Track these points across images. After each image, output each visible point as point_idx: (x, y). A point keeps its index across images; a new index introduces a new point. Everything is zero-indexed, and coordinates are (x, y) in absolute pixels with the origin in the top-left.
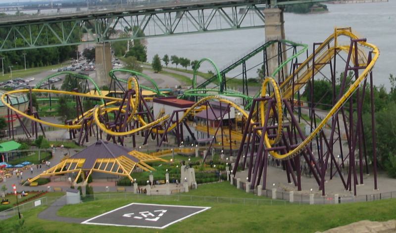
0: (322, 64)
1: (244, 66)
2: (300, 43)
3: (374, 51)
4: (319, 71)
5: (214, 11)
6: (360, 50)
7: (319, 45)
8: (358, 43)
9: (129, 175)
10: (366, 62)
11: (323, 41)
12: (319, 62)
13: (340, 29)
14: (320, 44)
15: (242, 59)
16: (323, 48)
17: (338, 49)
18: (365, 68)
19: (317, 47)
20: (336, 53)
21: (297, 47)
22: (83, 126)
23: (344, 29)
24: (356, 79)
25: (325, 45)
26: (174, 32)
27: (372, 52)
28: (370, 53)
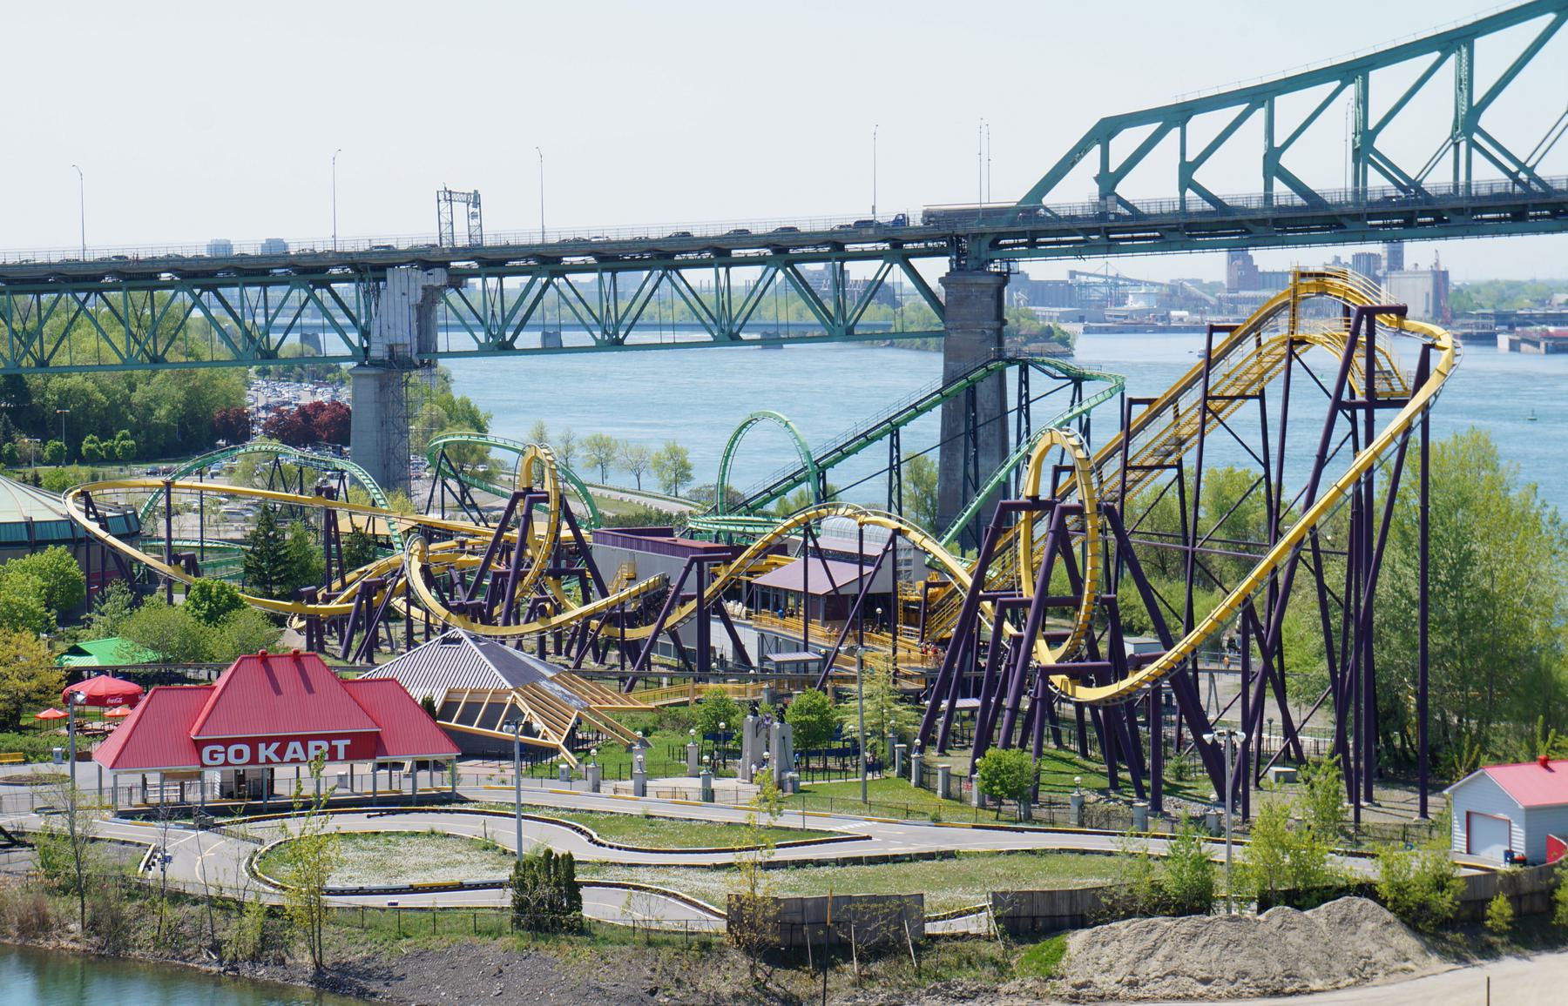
0: (1233, 398)
1: (895, 446)
2: (1095, 372)
3: (1439, 343)
4: (804, 815)
5: (772, 270)
6: (1380, 351)
7: (1146, 407)
8: (1377, 318)
9: (560, 744)
10: (1411, 385)
11: (1158, 392)
12: (1145, 476)
13: (1311, 275)
14: (1149, 402)
15: (888, 420)
16: (1157, 414)
17: (1302, 342)
18: (1402, 404)
19: (1138, 411)
20: (1291, 354)
21: (1084, 384)
22: (359, 605)
23: (1323, 275)
24: (1187, 634)
25: (1246, 335)
26: (627, 342)
27: (1433, 346)
28: (1426, 349)
